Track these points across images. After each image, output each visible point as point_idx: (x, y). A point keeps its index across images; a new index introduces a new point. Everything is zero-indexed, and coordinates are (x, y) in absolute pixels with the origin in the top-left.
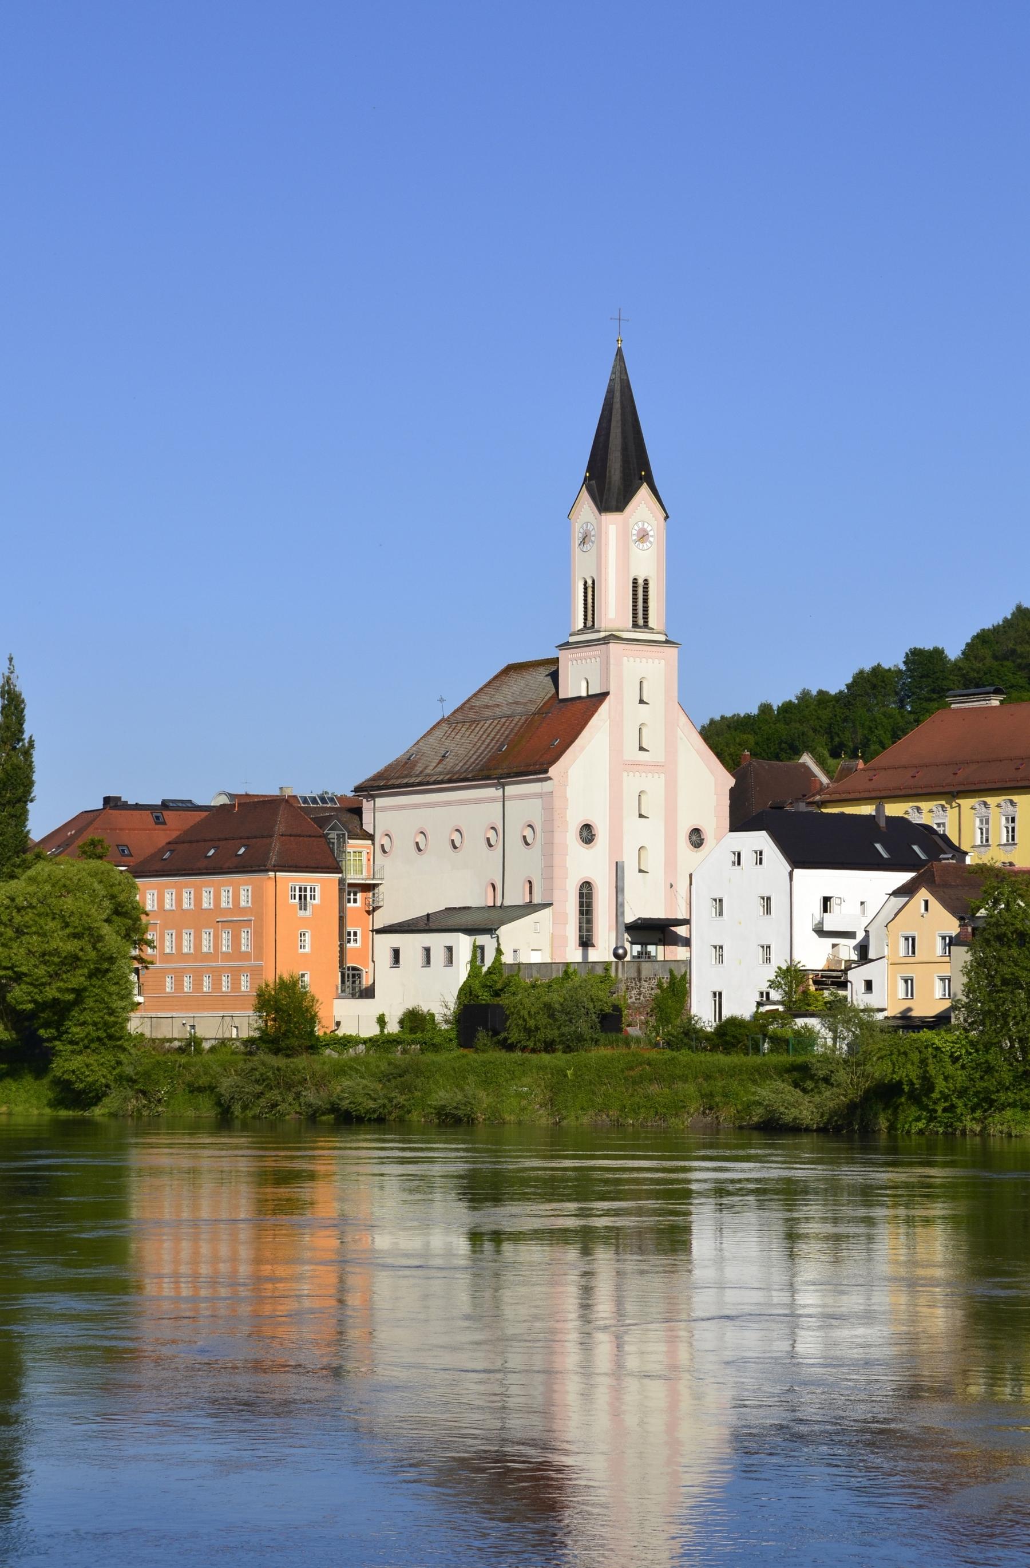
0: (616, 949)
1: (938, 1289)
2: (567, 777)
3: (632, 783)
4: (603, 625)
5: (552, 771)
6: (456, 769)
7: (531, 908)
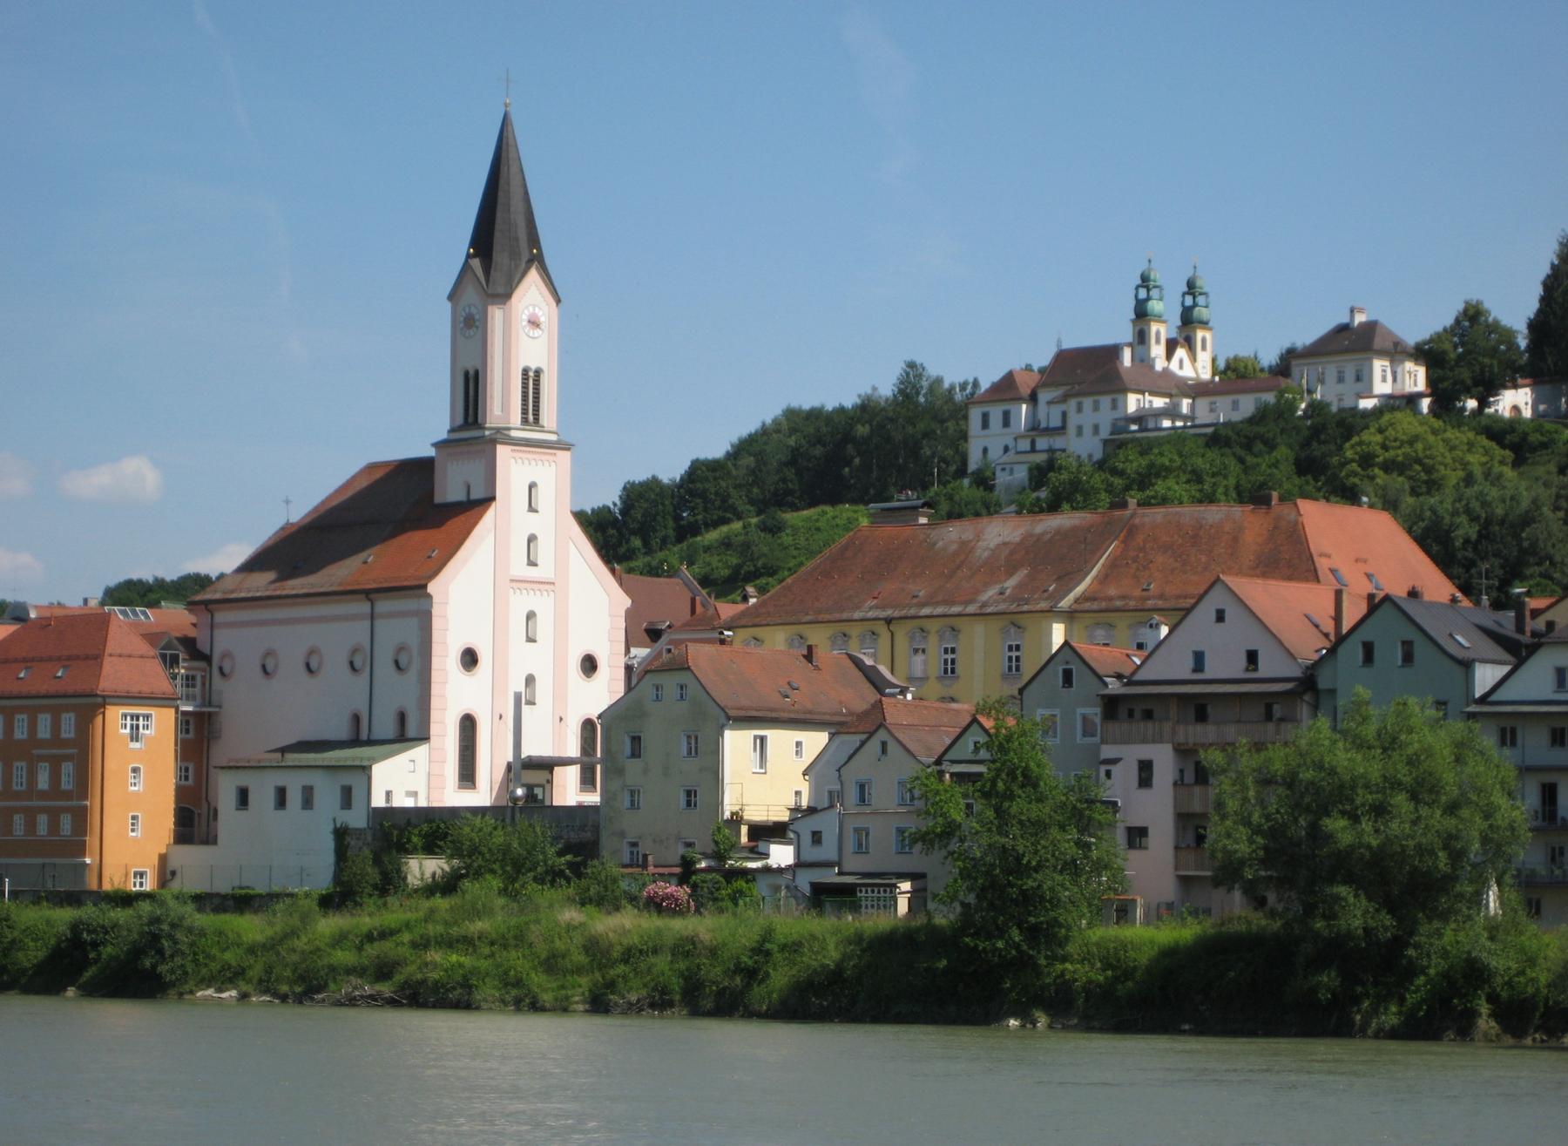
1: (703, 865)
3: (520, 603)
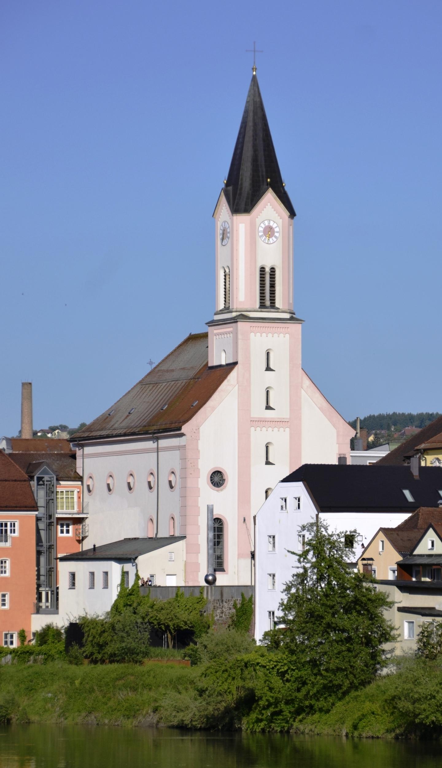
0: (207, 576)
2: (199, 433)
3: (259, 437)
4: (235, 307)
5: (185, 429)
6: (132, 424)
7: (173, 539)
